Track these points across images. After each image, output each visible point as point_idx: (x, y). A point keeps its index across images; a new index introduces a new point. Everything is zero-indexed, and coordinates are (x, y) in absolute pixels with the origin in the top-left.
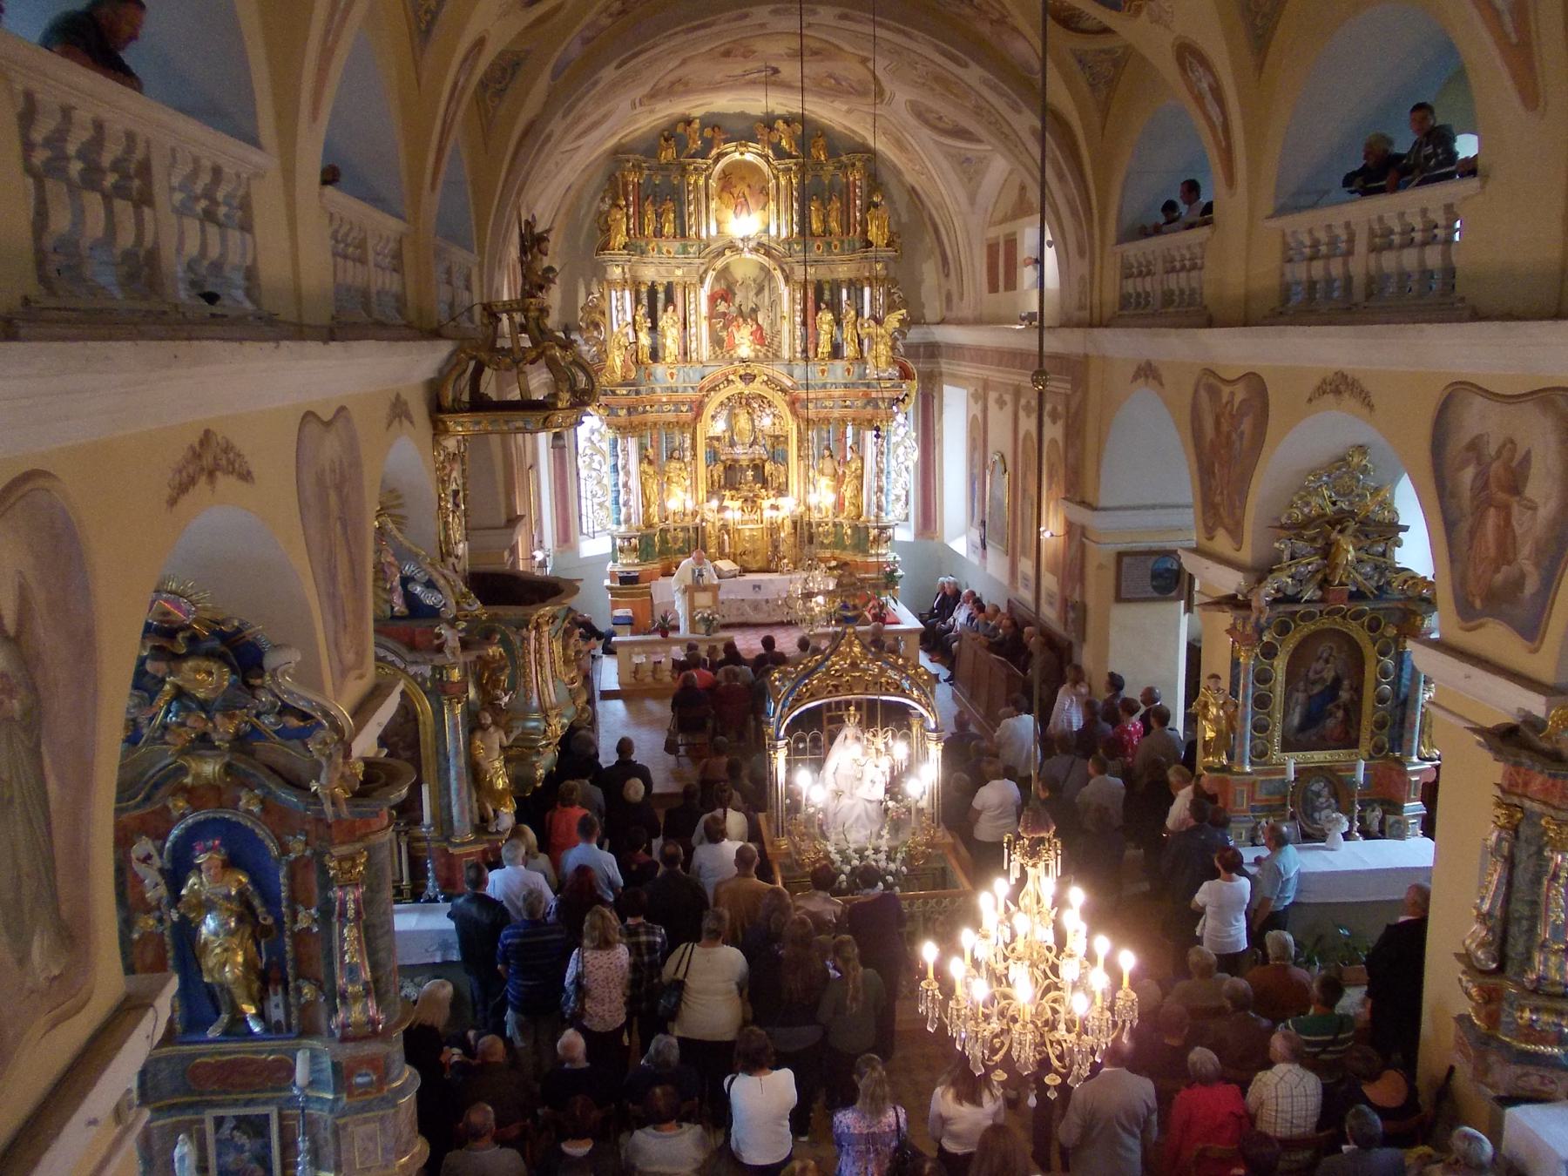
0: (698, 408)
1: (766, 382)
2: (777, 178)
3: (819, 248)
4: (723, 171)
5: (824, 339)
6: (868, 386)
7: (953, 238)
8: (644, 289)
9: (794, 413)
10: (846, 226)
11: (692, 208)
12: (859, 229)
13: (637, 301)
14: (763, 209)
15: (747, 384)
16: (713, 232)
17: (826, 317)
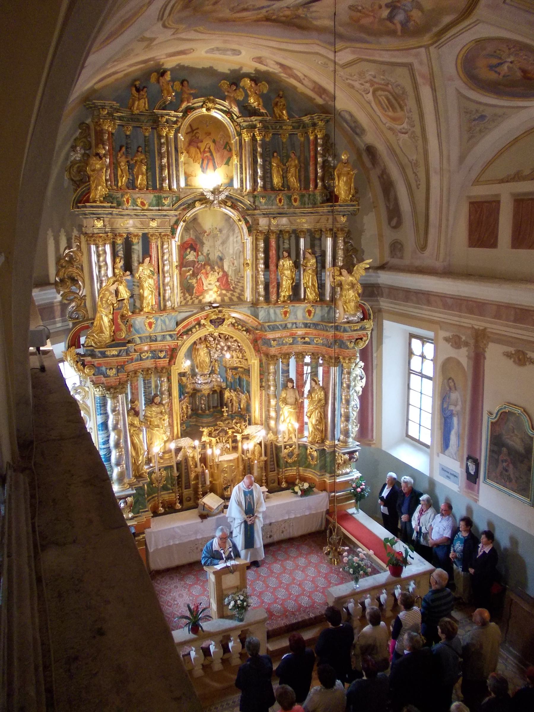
0: (173, 353)
1: (233, 325)
2: (239, 134)
3: (280, 201)
4: (190, 126)
5: (286, 284)
6: (337, 328)
7: (420, 195)
8: (119, 241)
9: (257, 350)
10: (305, 182)
11: (165, 161)
12: (320, 184)
13: (114, 255)
14: (227, 163)
15: (216, 327)
16: (182, 184)
17: (287, 263)
